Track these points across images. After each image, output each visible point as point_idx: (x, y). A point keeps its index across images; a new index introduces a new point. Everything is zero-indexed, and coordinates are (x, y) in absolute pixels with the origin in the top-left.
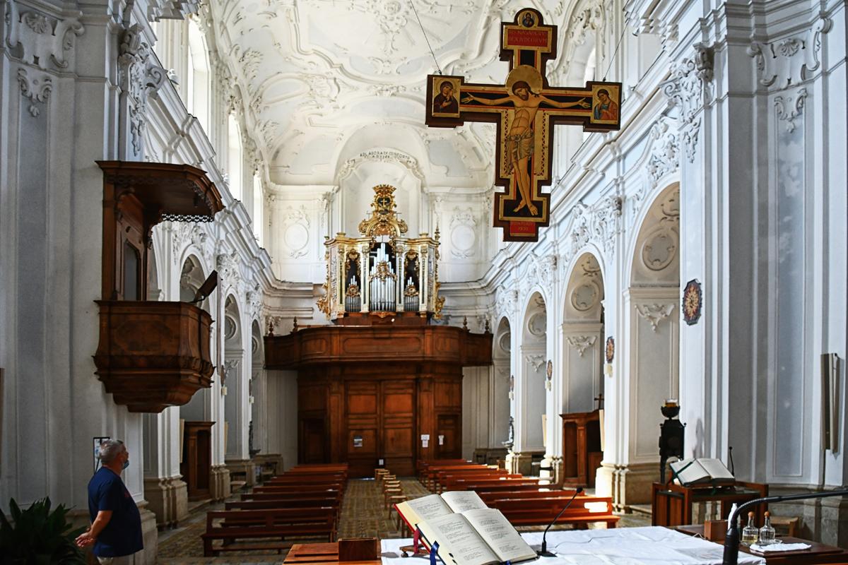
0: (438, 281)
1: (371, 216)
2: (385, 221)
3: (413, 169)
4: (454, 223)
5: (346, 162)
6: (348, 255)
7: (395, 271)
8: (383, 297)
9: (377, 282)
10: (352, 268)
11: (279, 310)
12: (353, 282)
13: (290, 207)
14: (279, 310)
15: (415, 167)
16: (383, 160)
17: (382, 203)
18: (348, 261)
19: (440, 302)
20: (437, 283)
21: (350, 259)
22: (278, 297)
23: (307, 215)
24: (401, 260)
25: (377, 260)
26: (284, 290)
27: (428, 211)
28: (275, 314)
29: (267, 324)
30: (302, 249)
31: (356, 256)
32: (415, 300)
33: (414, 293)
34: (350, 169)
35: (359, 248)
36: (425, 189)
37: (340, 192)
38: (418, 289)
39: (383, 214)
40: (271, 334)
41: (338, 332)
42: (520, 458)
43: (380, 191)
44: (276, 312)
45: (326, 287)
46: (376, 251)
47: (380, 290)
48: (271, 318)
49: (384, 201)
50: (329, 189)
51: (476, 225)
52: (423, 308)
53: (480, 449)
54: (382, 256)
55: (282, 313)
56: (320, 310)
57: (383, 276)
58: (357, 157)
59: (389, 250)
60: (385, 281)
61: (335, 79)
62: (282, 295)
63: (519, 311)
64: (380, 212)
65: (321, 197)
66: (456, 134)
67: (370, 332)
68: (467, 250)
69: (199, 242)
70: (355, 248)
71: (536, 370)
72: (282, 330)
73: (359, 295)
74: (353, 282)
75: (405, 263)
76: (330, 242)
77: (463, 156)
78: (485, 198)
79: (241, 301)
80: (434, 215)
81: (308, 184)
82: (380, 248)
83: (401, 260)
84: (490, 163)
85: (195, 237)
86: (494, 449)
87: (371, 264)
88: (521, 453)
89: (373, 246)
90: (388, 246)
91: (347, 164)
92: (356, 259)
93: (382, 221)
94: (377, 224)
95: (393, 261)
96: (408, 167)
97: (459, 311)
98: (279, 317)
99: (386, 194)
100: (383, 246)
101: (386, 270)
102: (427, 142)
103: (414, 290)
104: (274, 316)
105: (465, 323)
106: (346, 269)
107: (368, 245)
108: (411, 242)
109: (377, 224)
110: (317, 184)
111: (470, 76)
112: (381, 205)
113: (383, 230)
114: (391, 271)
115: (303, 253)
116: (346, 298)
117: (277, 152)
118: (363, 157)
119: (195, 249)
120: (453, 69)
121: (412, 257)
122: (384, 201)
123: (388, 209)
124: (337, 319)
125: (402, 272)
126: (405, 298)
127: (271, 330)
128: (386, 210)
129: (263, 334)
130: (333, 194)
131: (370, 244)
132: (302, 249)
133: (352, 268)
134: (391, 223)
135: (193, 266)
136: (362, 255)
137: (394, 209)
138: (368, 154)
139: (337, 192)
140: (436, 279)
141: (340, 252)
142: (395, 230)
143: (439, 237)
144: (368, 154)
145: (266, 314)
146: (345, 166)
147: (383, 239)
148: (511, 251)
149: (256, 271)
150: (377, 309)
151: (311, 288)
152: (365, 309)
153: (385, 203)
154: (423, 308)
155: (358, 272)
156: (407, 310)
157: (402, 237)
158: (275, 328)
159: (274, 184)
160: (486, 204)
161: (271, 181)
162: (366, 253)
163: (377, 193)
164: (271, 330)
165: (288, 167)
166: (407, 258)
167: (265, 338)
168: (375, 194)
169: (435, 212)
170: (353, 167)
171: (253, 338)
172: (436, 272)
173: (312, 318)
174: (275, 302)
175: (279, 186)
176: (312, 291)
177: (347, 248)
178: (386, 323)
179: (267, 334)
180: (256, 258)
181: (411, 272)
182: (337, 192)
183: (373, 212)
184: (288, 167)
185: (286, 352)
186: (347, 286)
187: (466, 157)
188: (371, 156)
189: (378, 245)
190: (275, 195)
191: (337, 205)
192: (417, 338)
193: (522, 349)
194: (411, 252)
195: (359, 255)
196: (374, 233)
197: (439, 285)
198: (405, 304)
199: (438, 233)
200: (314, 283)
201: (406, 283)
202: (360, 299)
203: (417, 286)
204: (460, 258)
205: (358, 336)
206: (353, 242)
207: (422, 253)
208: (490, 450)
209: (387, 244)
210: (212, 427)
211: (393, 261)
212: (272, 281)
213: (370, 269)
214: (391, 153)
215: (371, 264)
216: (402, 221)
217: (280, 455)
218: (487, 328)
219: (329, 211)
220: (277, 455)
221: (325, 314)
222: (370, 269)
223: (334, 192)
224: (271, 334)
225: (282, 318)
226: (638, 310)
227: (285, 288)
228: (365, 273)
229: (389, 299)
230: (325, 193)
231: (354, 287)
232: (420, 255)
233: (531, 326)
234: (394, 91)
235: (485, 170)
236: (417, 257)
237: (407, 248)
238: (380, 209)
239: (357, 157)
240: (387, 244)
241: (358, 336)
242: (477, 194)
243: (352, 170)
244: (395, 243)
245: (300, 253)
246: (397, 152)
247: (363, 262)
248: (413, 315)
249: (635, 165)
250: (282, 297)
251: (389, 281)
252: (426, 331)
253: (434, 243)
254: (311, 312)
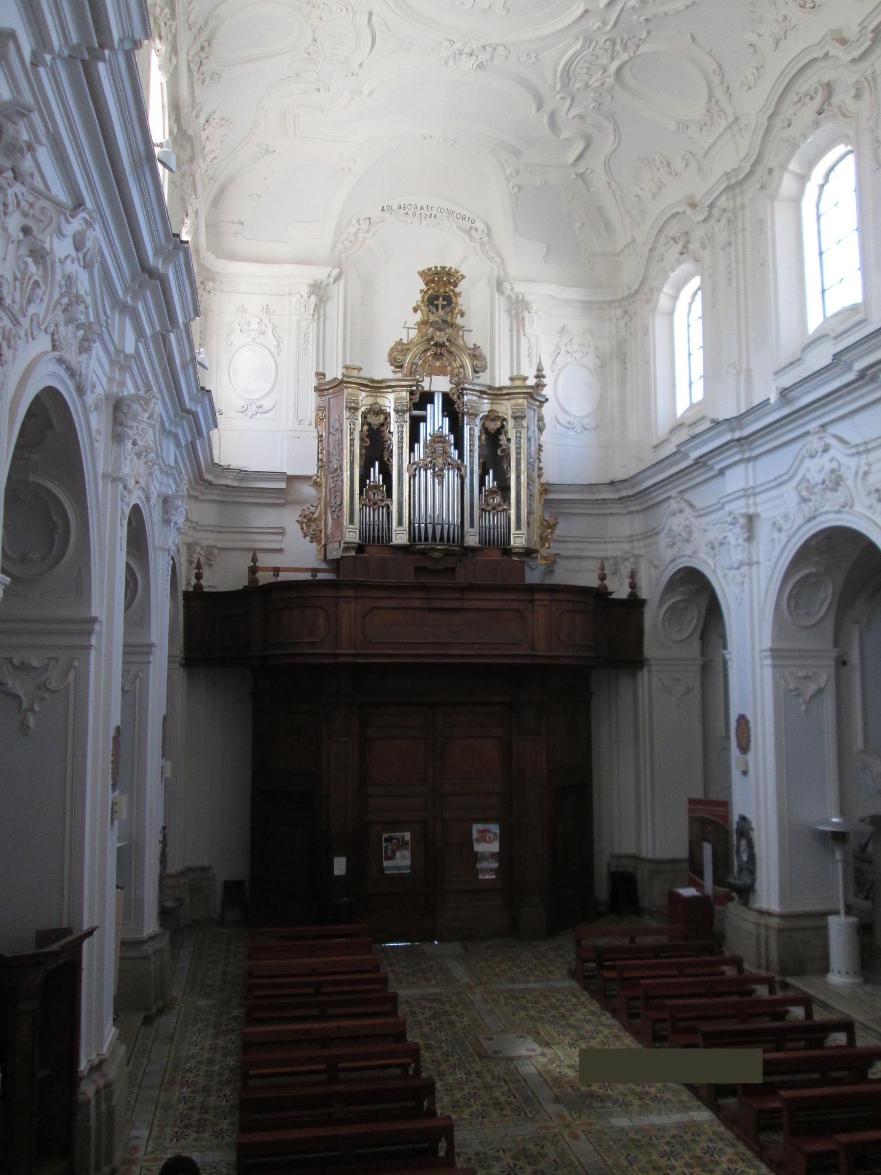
0: (544, 480)
1: (414, 333)
2: (442, 345)
3: (483, 244)
4: (559, 359)
5: (354, 222)
6: (364, 416)
7: (461, 456)
8: (430, 512)
9: (426, 477)
10: (375, 448)
11: (219, 530)
12: (375, 475)
13: (243, 309)
14: (219, 530)
15: (486, 239)
16: (424, 222)
17: (437, 306)
18: (366, 428)
19: (551, 527)
20: (542, 485)
21: (369, 424)
22: (214, 501)
23: (274, 327)
24: (472, 432)
25: (426, 431)
26: (227, 486)
27: (511, 331)
28: (208, 539)
29: (190, 562)
30: (265, 396)
31: (382, 417)
32: (500, 519)
33: (499, 505)
34: (361, 236)
35: (389, 401)
36: (507, 286)
37: (342, 283)
38: (506, 498)
39: (440, 330)
40: (198, 587)
41: (351, 593)
42: (780, 931)
43: (433, 281)
44: (209, 535)
45: (317, 485)
46: (425, 409)
47: (429, 496)
48: (198, 549)
49: (441, 302)
50: (321, 273)
51: (602, 366)
52: (518, 540)
53: (619, 857)
54: (435, 420)
55: (221, 536)
56: (305, 536)
57: (437, 462)
58: (376, 213)
59: (451, 409)
60: (442, 477)
61: (370, 14)
62: (221, 498)
63: (758, 563)
64: (432, 324)
65: (304, 290)
66: (573, 176)
67: (420, 594)
68: (584, 417)
69: (75, 348)
70: (381, 401)
71: (803, 708)
72: (226, 577)
73: (388, 507)
74: (375, 475)
75: (480, 437)
76: (327, 388)
77: (578, 225)
78: (619, 312)
79: (153, 518)
80: (523, 339)
81: (279, 262)
82: (432, 402)
83: (472, 432)
84: (634, 240)
85: (62, 329)
86: (653, 861)
87: (414, 437)
88: (782, 916)
89: (417, 398)
90: (447, 398)
91: (356, 225)
92: (382, 425)
93: (437, 345)
94: (426, 351)
95: (456, 428)
96: (472, 239)
97: (571, 546)
98: (215, 547)
99: (445, 286)
100: (438, 400)
101: (445, 453)
102: (516, 190)
103: (497, 499)
104: (205, 543)
105: (603, 578)
106: (361, 446)
107: (405, 394)
108: (496, 394)
109: (426, 351)
110: (296, 263)
111: (649, 33)
112: (434, 310)
113: (438, 364)
114: (454, 453)
115: (266, 408)
116: (361, 509)
117: (222, 190)
118: (387, 214)
119: (61, 371)
120: (622, 10)
121: (493, 426)
122: (441, 302)
123: (449, 319)
124: (342, 557)
125: (472, 458)
126: (480, 516)
127: (199, 576)
128: (445, 322)
129: (182, 586)
130: (328, 285)
131: (412, 393)
132: (265, 396)
133: (375, 448)
134: (453, 349)
135: (51, 427)
136: (393, 415)
137: (459, 321)
138: (395, 207)
139: (335, 282)
140: (540, 476)
141: (350, 409)
142: (462, 367)
143: (544, 386)
144: (395, 207)
145: (189, 540)
146: (353, 230)
147: (440, 384)
148: (749, 424)
149: (183, 443)
150: (426, 539)
151: (282, 485)
152: (400, 537)
153: (443, 307)
154: (518, 540)
155: (386, 453)
156: (486, 542)
157: (476, 381)
158: (206, 571)
159: (214, 257)
160: (622, 324)
161: (207, 250)
162: (404, 412)
163: (426, 284)
164: (199, 576)
165: (242, 223)
166: (485, 430)
167: (186, 594)
168: (424, 288)
169: (524, 335)
170: (367, 232)
171: (129, 567)
172: (540, 462)
173: (281, 550)
174: (207, 514)
175: (224, 261)
176: (280, 490)
177: (364, 399)
178: (439, 566)
179: (188, 584)
180: (188, 412)
181: (494, 456)
182: (335, 282)
183: (418, 324)
184: (242, 223)
185: (236, 633)
186: (363, 485)
187: (583, 226)
188: (402, 212)
189: (427, 398)
190: (213, 280)
191: (335, 309)
192: (516, 611)
193: (774, 657)
194: (491, 416)
195: (387, 416)
196: (420, 369)
197: (546, 488)
198: (480, 528)
199: (543, 377)
200: (289, 473)
201: (482, 483)
202: (389, 514)
203: (503, 488)
204: (571, 432)
205: (393, 603)
206: (376, 387)
207: (515, 418)
208: (645, 860)
209: (446, 396)
210: (86, 944)
211: (456, 428)
212: (207, 467)
213: (412, 449)
214: (441, 210)
215: (414, 437)
216: (476, 347)
217: (209, 868)
218: (633, 586)
219: (319, 318)
220: (203, 869)
221: (315, 544)
222: (412, 449)
223: (331, 280)
224: (198, 587)
225: (220, 549)
226: (782, 681)
227: (229, 482)
228: (400, 455)
229: (450, 514)
230: (312, 281)
231: (376, 487)
232: (510, 424)
233: (793, 603)
234: (483, 57)
235: (618, 255)
236: (503, 426)
237: (485, 406)
238: (432, 318)
239: (376, 213)
240: (446, 396)
241: (393, 603)
242: (603, 302)
243: (364, 238)
244: (461, 395)
245: (260, 407)
246: (452, 207)
247: (397, 431)
248: (495, 556)
249: (775, 479)
250: (220, 502)
251: (450, 476)
252: (537, 596)
253: (534, 394)
254: (279, 537)
